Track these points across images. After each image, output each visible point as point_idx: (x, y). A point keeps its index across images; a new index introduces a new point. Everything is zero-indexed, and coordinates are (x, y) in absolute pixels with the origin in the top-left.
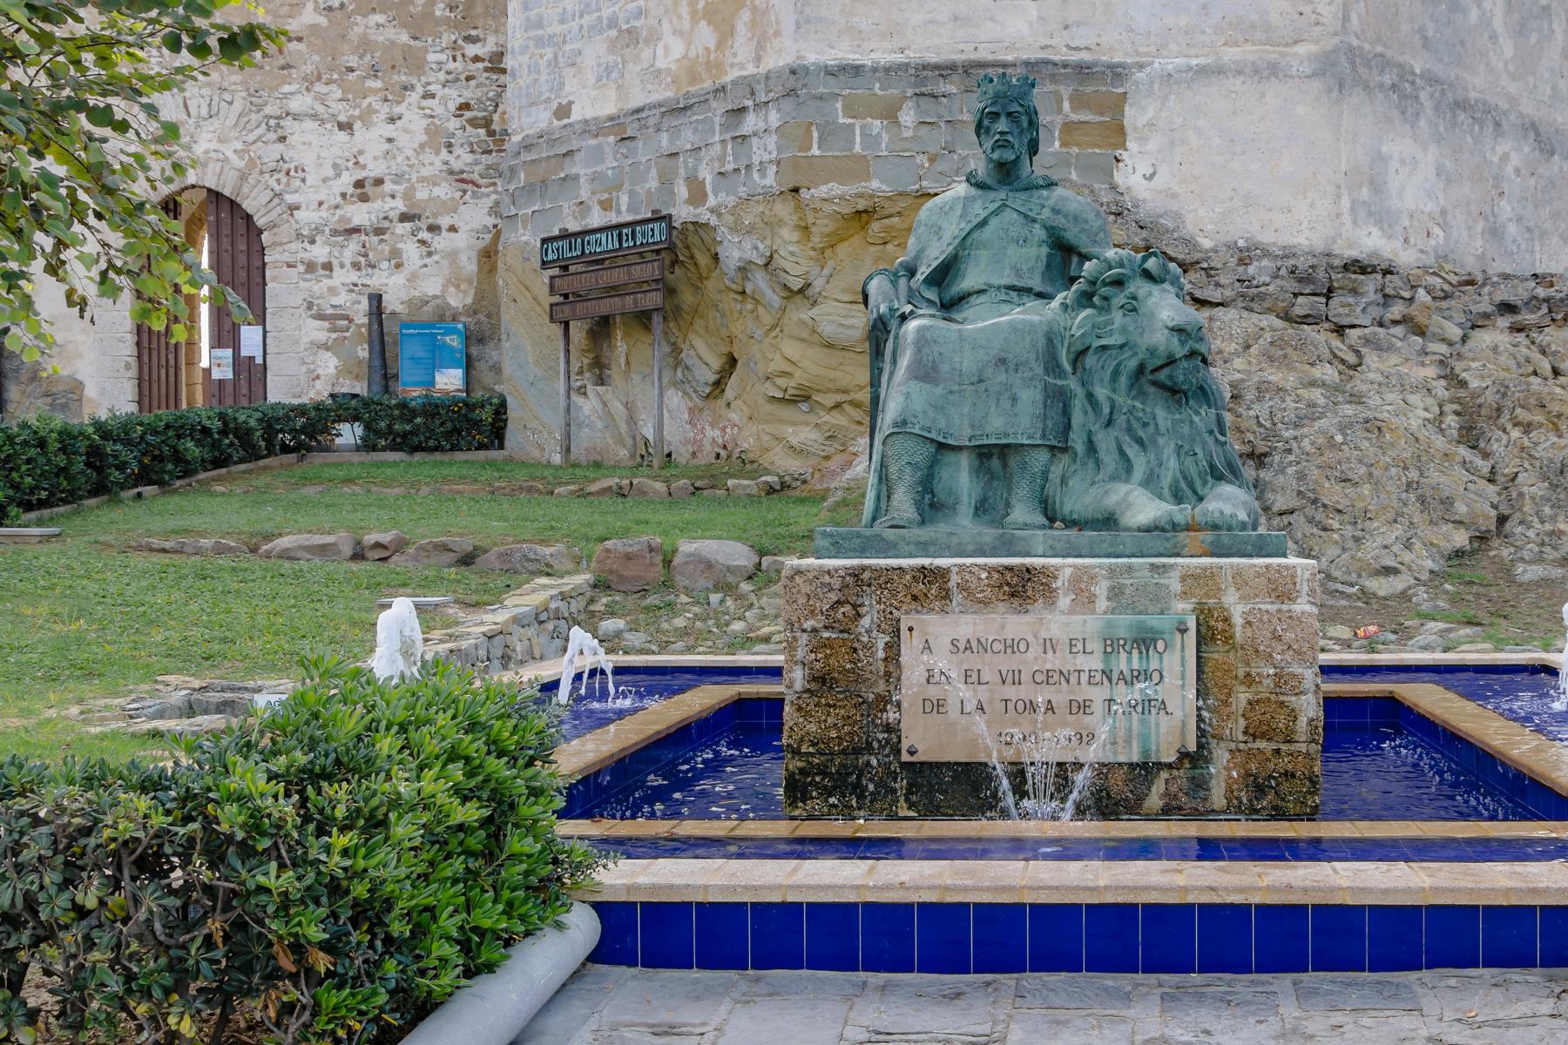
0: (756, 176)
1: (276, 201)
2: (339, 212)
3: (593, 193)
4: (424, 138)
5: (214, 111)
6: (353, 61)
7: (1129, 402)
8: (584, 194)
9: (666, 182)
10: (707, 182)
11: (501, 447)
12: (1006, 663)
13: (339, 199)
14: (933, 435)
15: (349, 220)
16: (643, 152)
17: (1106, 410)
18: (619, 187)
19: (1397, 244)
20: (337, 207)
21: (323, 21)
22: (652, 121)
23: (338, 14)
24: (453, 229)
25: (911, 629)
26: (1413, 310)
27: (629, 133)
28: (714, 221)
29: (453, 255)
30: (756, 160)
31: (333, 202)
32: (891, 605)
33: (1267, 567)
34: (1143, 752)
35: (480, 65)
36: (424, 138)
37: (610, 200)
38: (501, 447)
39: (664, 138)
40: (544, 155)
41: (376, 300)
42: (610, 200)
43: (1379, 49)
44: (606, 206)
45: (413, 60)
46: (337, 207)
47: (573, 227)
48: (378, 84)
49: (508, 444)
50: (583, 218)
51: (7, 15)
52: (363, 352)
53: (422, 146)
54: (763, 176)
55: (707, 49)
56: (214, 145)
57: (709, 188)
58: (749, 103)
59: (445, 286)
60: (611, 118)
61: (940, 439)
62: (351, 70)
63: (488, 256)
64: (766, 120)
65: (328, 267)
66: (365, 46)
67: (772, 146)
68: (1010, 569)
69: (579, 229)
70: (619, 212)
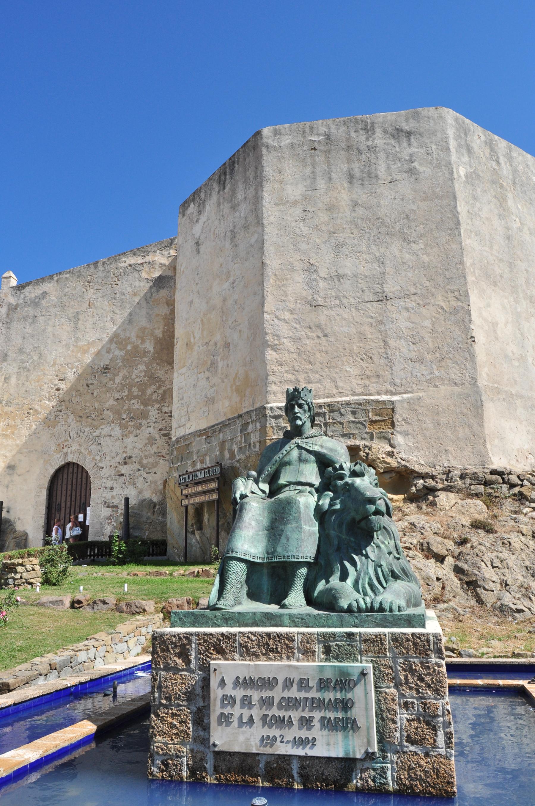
0: (252, 447)
1: (96, 466)
2: (117, 469)
3: (198, 457)
4: (147, 442)
5: (78, 435)
6: (124, 416)
7: (348, 538)
8: (195, 457)
9: (222, 451)
10: (236, 450)
11: (166, 555)
12: (266, 694)
13: (117, 464)
14: (247, 558)
15: (120, 471)
16: (215, 442)
17: (336, 542)
18: (206, 455)
19: (513, 462)
20: (116, 467)
21: (115, 403)
22: (218, 430)
23: (121, 401)
24: (155, 473)
25: (215, 670)
26: (523, 489)
27: (210, 435)
28: (238, 465)
29: (155, 482)
30: (252, 442)
31: (115, 465)
32: (206, 655)
33: (413, 634)
34: (345, 751)
35: (167, 415)
36: (147, 442)
37: (203, 460)
38: (166, 555)
39: (221, 436)
40: (182, 444)
41: (127, 500)
42: (203, 460)
43: (496, 386)
44: (202, 462)
45: (144, 415)
46: (116, 467)
47: (190, 470)
48: (132, 423)
49: (168, 554)
50: (194, 467)
51: (531, 484)
52: (122, 519)
53: (146, 444)
54: (254, 448)
55: (236, 402)
56: (78, 447)
57: (236, 454)
58: (250, 420)
59: (152, 494)
60: (204, 430)
61: (251, 559)
62: (124, 419)
63: (165, 482)
64: (256, 427)
65: (112, 488)
66: (129, 411)
67: (258, 436)
68: (268, 635)
69: (192, 470)
70: (206, 464)
